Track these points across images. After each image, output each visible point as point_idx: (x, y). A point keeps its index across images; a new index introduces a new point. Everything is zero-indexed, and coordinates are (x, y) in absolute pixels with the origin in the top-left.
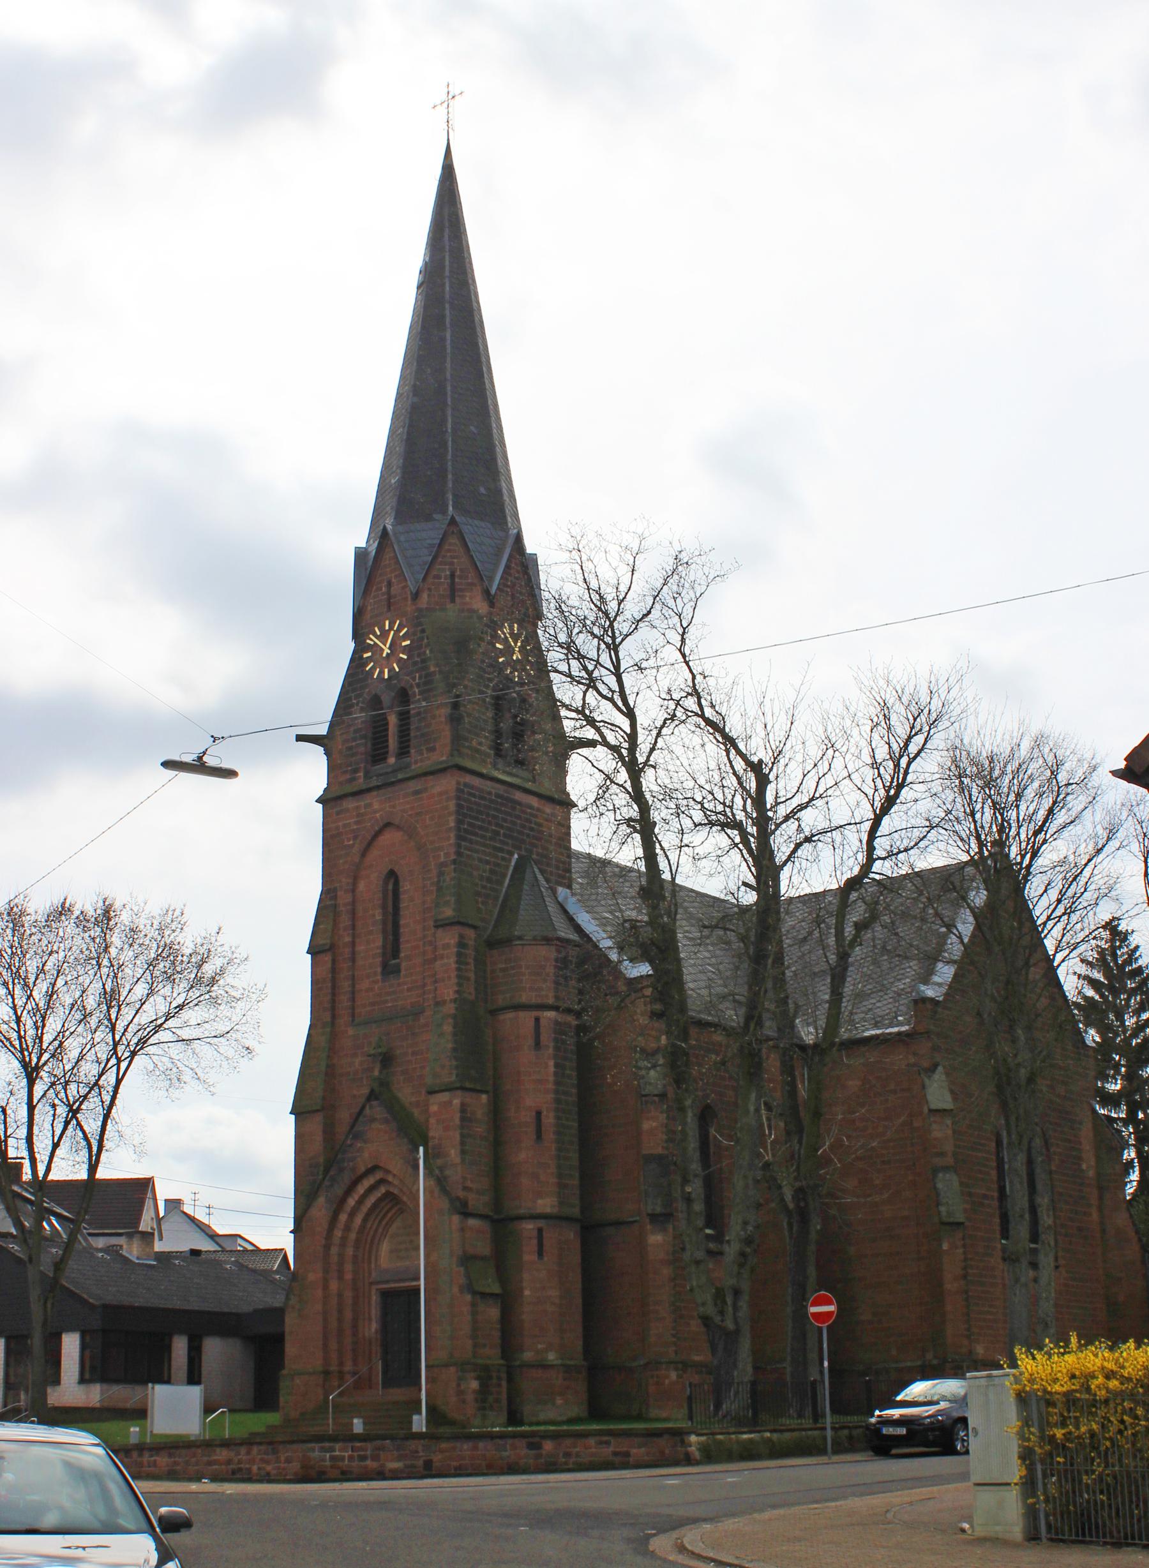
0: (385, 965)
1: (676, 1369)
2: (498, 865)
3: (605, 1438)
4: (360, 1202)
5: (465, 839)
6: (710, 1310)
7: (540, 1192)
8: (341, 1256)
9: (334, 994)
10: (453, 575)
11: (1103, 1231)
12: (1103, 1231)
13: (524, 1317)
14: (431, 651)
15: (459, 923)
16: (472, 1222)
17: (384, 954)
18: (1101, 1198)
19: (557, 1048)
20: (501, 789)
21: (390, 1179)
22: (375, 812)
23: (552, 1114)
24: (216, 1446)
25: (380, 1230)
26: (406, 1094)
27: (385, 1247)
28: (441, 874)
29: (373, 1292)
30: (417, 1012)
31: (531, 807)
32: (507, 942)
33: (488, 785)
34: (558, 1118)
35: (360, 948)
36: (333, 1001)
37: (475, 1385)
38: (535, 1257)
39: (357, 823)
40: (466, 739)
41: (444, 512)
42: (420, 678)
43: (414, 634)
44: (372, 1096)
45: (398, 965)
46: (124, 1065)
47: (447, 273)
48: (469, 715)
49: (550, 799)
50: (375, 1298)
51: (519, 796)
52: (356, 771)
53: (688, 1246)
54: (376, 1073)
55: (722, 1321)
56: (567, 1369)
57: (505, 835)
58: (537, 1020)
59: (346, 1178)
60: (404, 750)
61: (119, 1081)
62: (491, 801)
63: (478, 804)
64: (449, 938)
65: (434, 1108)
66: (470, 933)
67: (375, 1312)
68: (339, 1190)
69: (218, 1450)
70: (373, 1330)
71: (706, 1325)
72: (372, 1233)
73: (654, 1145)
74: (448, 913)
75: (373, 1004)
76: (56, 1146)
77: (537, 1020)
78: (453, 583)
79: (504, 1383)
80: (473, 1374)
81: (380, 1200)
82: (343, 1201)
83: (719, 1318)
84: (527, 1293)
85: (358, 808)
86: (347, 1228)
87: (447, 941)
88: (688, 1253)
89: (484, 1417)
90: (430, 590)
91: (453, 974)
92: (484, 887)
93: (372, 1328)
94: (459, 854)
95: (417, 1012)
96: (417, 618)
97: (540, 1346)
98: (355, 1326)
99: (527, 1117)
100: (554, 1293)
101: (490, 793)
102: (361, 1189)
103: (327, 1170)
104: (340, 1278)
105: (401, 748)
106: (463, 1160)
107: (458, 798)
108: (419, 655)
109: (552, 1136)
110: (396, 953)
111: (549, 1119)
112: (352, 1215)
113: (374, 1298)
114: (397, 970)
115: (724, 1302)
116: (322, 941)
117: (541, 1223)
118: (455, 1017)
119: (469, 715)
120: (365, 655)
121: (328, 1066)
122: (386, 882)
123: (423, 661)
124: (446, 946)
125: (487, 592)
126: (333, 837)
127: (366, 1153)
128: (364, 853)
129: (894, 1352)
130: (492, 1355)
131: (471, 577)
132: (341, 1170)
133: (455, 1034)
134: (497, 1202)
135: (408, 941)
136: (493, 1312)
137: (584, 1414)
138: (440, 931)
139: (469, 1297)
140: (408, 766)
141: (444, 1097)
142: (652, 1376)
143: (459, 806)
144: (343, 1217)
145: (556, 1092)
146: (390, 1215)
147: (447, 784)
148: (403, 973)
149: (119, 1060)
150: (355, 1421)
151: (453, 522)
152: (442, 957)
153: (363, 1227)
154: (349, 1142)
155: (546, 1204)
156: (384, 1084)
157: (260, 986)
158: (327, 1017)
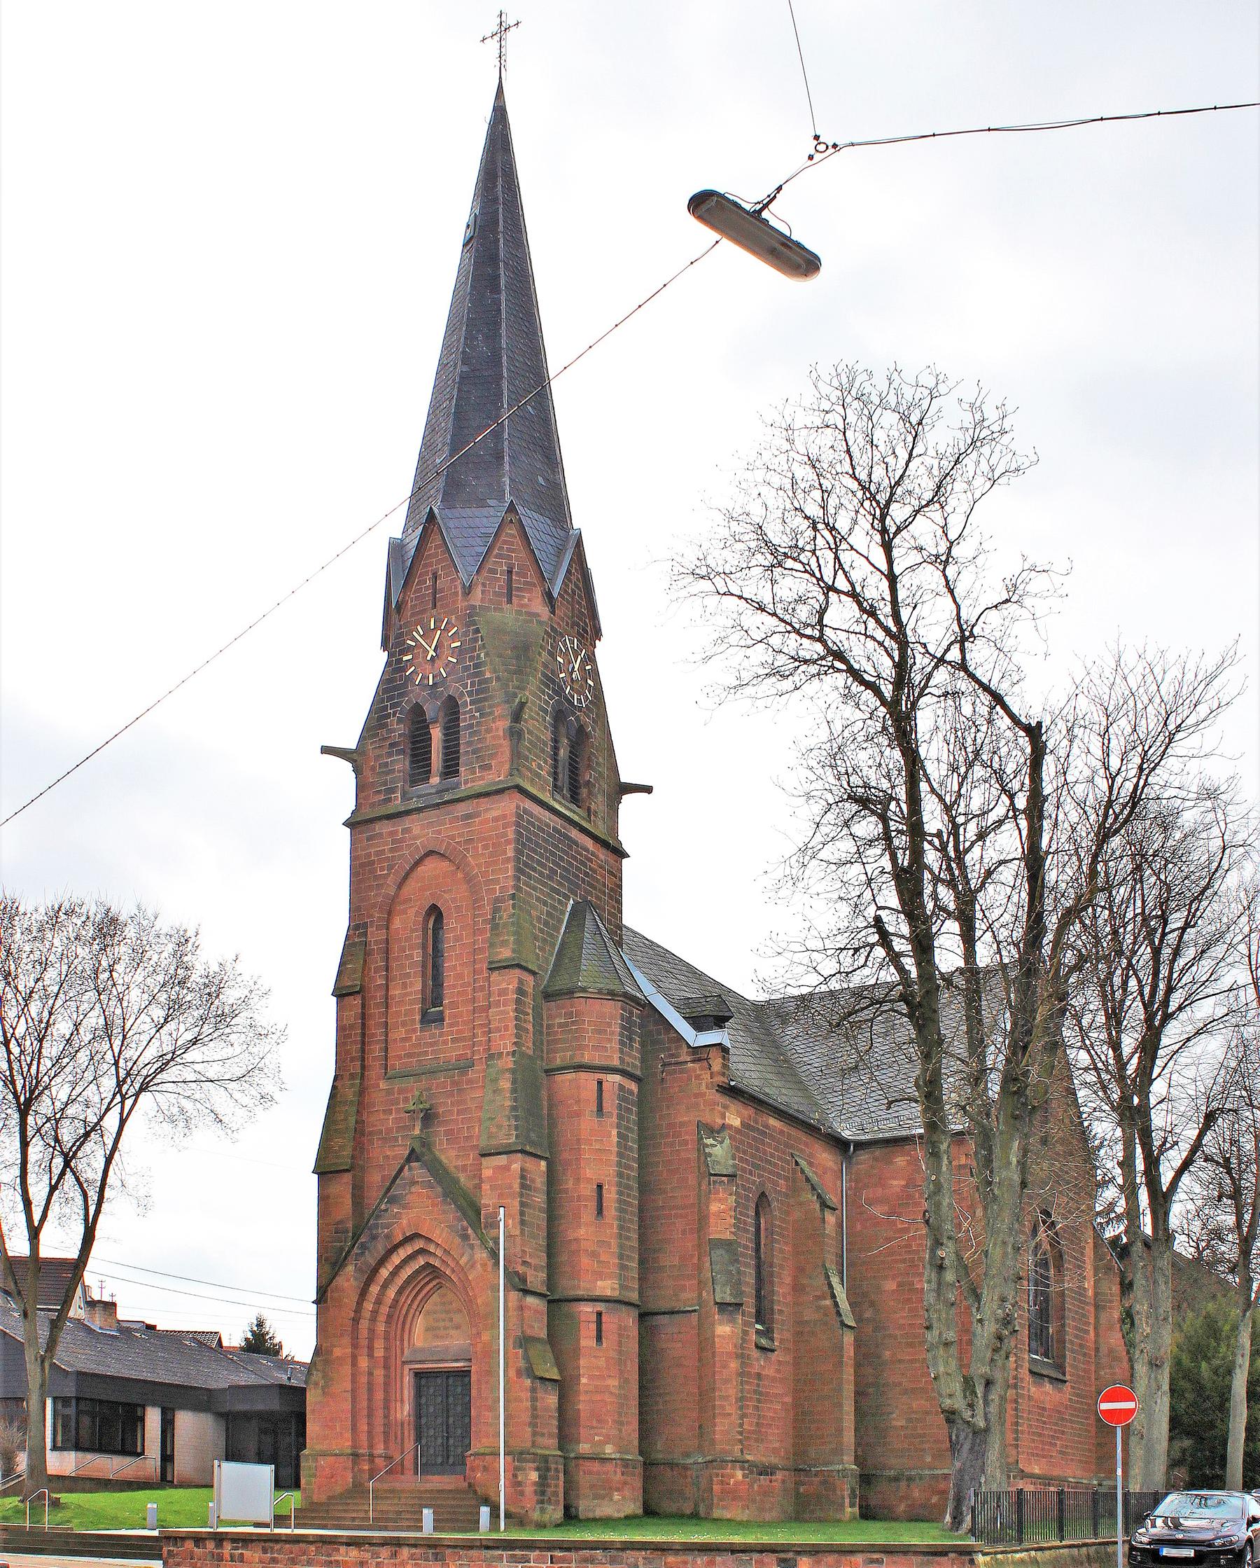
0: (424, 1014)
1: (743, 1469)
2: (554, 908)
3: (875, 1556)
4: (394, 1273)
5: (523, 872)
6: (959, 1403)
7: (601, 1270)
8: (372, 1331)
9: (363, 1043)
10: (510, 572)
11: (1097, 1350)
12: (1097, 1350)
13: (581, 1407)
14: (487, 655)
15: (519, 966)
16: (530, 1300)
17: (424, 1000)
18: (1096, 1317)
19: (620, 1117)
20: (559, 823)
21: (432, 1248)
22: (416, 838)
23: (614, 1189)
24: (342, 1544)
25: (415, 1306)
26: (449, 1156)
27: (420, 1324)
28: (496, 910)
29: (406, 1371)
30: (464, 1066)
31: (587, 850)
32: (570, 993)
33: (546, 816)
34: (620, 1193)
35: (395, 992)
36: (363, 1051)
37: (534, 1476)
38: (593, 1343)
39: (392, 850)
40: (527, 759)
41: (501, 498)
42: (473, 685)
43: (466, 634)
44: (412, 1156)
45: (442, 1012)
46: (129, 1103)
47: (501, 228)
48: (530, 732)
49: (605, 844)
50: (408, 1379)
51: (574, 834)
52: (392, 790)
53: (935, 1325)
54: (417, 1132)
55: (973, 1416)
56: (626, 1463)
57: (562, 876)
58: (600, 1083)
59: (380, 1247)
60: (451, 769)
61: (123, 1122)
62: (549, 835)
63: (536, 835)
64: (507, 982)
65: (487, 1173)
66: (530, 980)
67: (408, 1392)
68: (371, 1260)
69: (343, 1549)
70: (405, 1413)
71: (948, 1421)
72: (405, 1309)
73: (721, 1229)
74: (506, 953)
75: (410, 1055)
76: (53, 1189)
77: (600, 1083)
78: (510, 580)
79: (561, 1475)
80: (531, 1465)
81: (417, 1272)
82: (375, 1271)
83: (970, 1413)
84: (584, 1380)
85: (391, 834)
86: (379, 1302)
87: (504, 986)
88: (936, 1332)
89: (543, 1510)
90: (484, 585)
91: (512, 1024)
92: (541, 931)
93: (404, 1410)
94: (518, 888)
95: (464, 1066)
96: (470, 616)
97: (597, 1438)
98: (387, 1407)
99: (588, 1190)
100: (613, 1383)
101: (548, 826)
102: (396, 1259)
103: (356, 1237)
104: (371, 1355)
105: (446, 767)
106: (522, 1231)
107: (518, 825)
108: (471, 658)
109: (614, 1212)
110: (437, 1000)
111: (610, 1195)
112: (385, 1286)
113: (406, 1379)
114: (440, 1019)
115: (974, 1393)
116: (352, 982)
117: (600, 1307)
118: (513, 1071)
119: (530, 732)
120: (405, 658)
121: (357, 1122)
122: (426, 921)
123: (476, 666)
124: (502, 992)
125: (549, 595)
126: (362, 865)
127: (403, 1220)
128: (400, 886)
129: (929, 1459)
130: (549, 1445)
131: (531, 576)
132: (374, 1238)
133: (514, 1091)
134: (551, 1282)
135: (454, 986)
136: (552, 1400)
137: (640, 1511)
138: (495, 976)
139: (528, 1382)
140: (458, 785)
141: (502, 1160)
142: (717, 1475)
143: (519, 834)
144: (374, 1289)
145: (619, 1164)
146: (428, 1288)
147: (507, 806)
148: (447, 1021)
149: (124, 1099)
150: (425, 1511)
151: (512, 509)
152: (498, 1004)
153: (396, 1301)
154: (383, 1207)
155: (606, 1287)
156: (426, 1143)
157: (281, 1026)
158: (356, 1067)
